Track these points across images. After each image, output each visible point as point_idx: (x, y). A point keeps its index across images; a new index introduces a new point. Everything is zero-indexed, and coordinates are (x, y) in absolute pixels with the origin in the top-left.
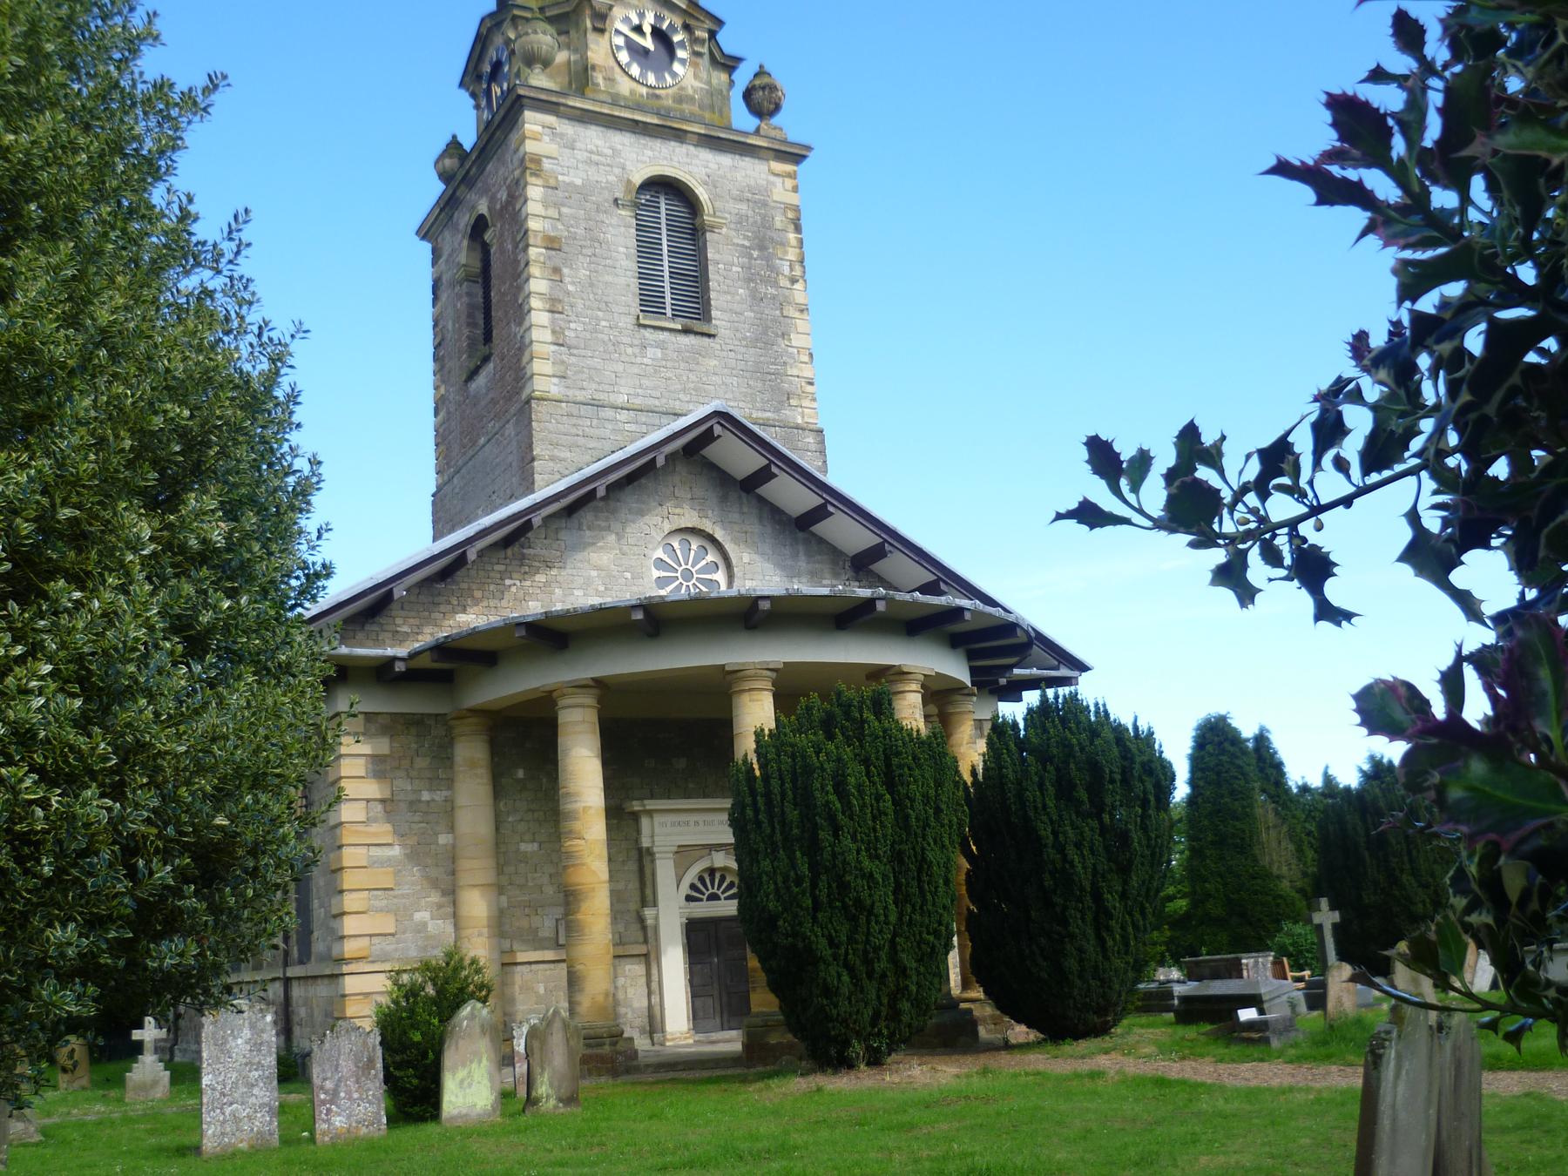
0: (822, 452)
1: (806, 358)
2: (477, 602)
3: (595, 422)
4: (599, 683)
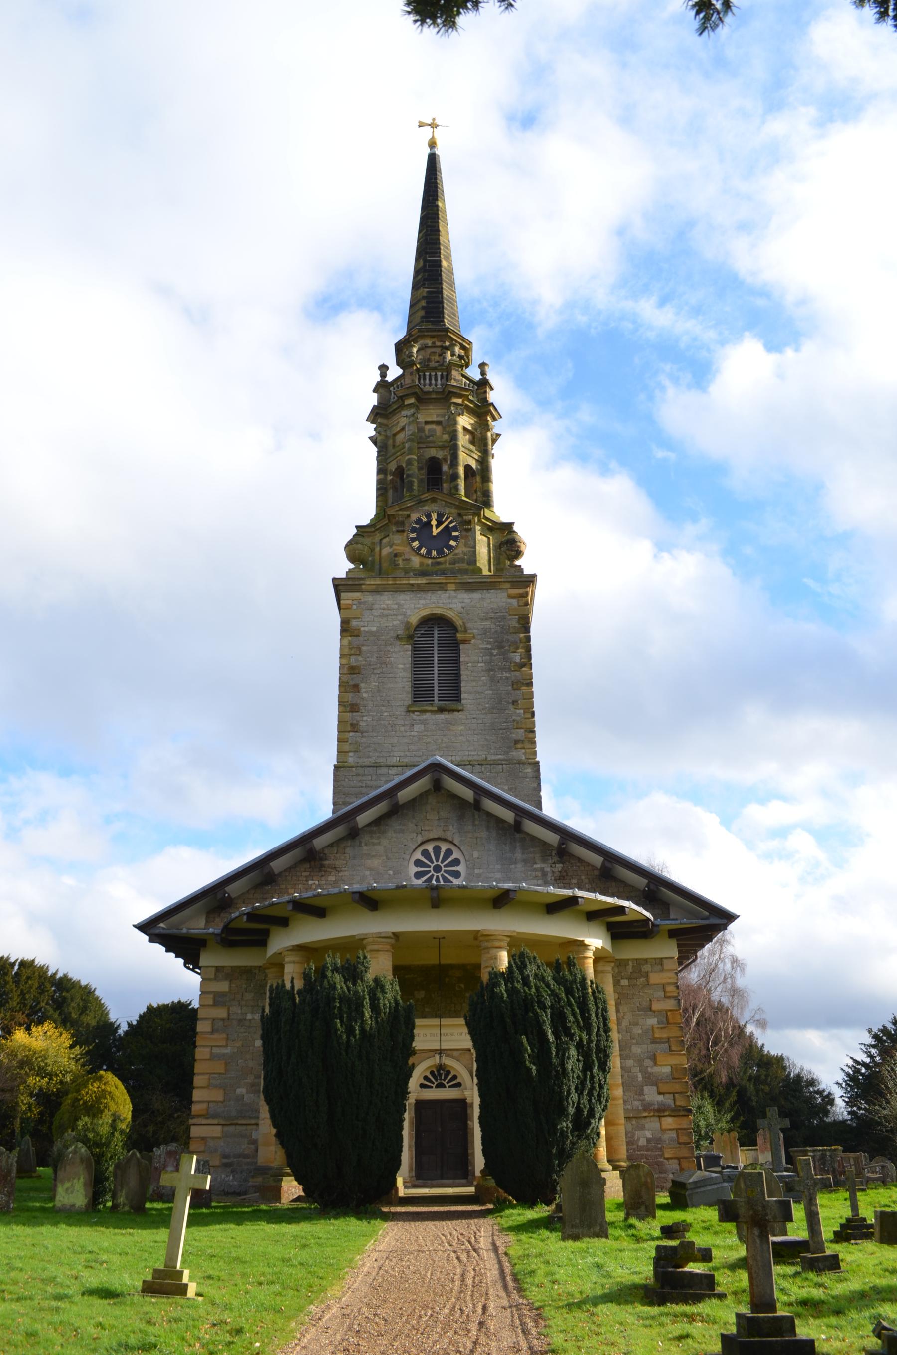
3: (374, 777)
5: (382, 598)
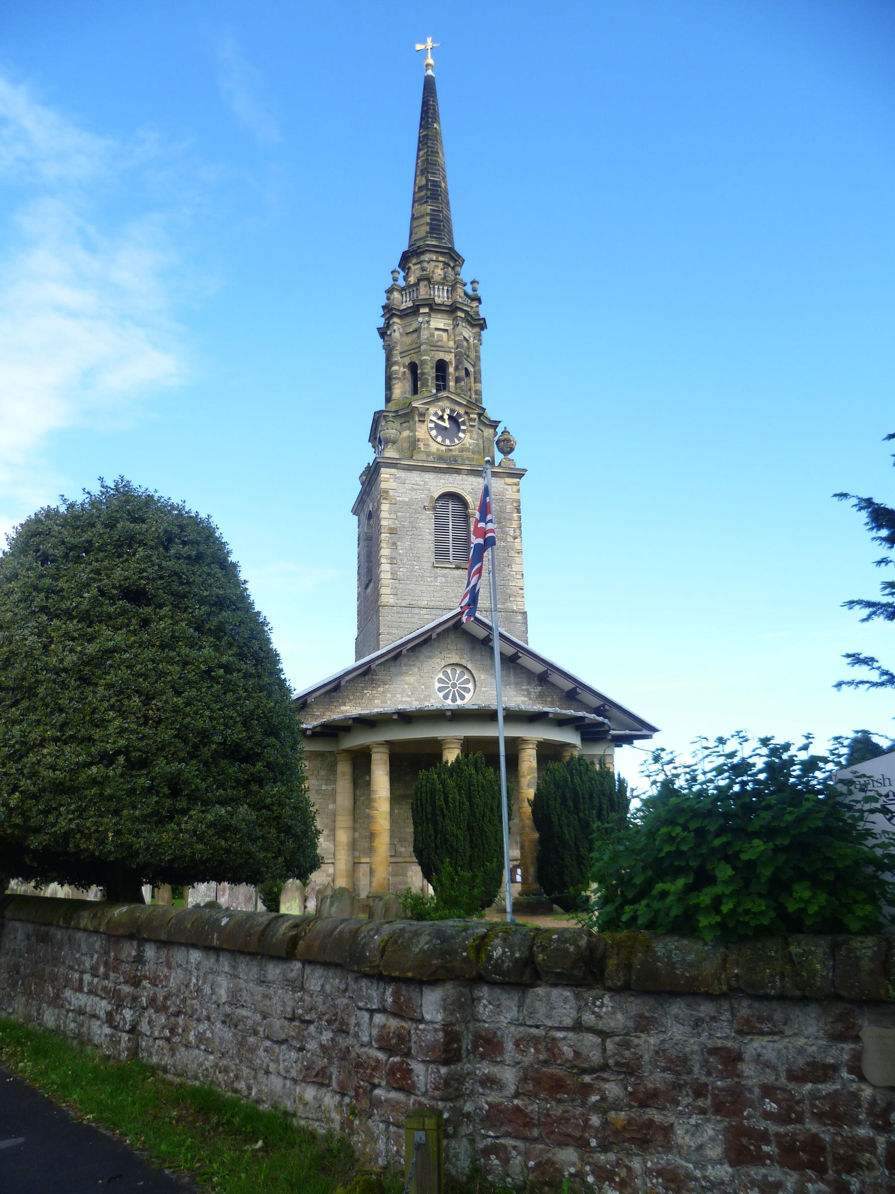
0: (526, 623)
1: (520, 577)
2: (350, 701)
4: (388, 743)
5: (412, 475)
